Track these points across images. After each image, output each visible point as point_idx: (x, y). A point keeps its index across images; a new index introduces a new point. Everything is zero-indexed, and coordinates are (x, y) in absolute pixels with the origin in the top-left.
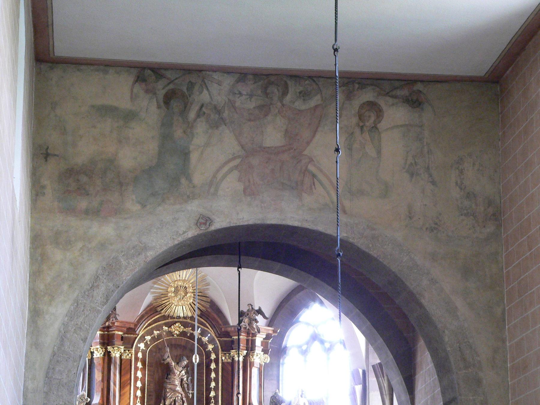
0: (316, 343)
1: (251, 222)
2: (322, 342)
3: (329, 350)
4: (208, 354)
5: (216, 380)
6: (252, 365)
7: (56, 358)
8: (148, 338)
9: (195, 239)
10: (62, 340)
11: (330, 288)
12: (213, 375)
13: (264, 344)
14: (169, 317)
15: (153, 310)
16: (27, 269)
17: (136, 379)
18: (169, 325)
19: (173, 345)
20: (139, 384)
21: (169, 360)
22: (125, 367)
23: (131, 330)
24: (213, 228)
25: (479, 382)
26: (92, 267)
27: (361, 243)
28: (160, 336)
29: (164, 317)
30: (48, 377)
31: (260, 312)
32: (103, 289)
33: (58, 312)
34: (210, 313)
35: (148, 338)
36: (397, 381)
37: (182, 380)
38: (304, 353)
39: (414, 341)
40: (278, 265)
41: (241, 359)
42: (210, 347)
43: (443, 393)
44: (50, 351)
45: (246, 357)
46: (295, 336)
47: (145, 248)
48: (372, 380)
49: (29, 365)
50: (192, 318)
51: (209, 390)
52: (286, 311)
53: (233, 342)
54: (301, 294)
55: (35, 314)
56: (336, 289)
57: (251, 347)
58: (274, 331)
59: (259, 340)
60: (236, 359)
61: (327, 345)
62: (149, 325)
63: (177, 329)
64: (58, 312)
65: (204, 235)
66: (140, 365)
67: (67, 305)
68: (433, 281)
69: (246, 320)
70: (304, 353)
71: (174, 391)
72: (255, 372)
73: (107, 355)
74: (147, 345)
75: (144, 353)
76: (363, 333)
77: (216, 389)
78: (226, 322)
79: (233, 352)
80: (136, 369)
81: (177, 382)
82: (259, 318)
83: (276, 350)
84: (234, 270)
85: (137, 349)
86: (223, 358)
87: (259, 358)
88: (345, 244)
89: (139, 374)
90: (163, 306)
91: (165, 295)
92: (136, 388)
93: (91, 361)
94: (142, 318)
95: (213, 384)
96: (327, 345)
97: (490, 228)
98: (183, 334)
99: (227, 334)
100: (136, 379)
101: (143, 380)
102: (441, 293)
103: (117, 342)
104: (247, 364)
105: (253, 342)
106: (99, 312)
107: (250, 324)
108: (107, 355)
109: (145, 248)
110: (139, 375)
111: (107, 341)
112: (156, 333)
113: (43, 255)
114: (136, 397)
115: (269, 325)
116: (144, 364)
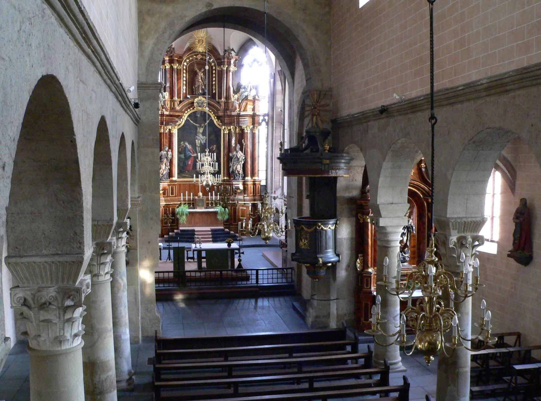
0: (256, 63)
1: (229, 6)
2: (258, 62)
3: (261, 65)
4: (212, 67)
5: (215, 77)
6: (230, 71)
7: (151, 61)
8: (188, 60)
9: (206, 12)
10: (152, 54)
11: (261, 37)
12: (214, 75)
13: (235, 63)
14: (196, 52)
15: (189, 49)
16: (137, 24)
17: (183, 77)
18: (196, 55)
19: (198, 64)
20: (185, 79)
21: (196, 69)
22: (179, 72)
23: (181, 57)
24: (213, 8)
25: (320, 71)
26: (163, 24)
27: (274, 15)
28: (192, 60)
29: (194, 52)
30: (147, 69)
31: (233, 50)
32: (168, 33)
33: (150, 43)
34: (213, 51)
35: (188, 60)
36: (287, 74)
37: (202, 77)
38: (250, 66)
39: (295, 58)
40: (240, 27)
41: (225, 69)
42: (213, 64)
43: (306, 76)
44: (148, 59)
45: (227, 68)
46: (247, 60)
47: (185, 16)
48: (278, 77)
49: (139, 64)
50: (205, 52)
51: (212, 81)
52: (243, 49)
53: (222, 62)
54: (249, 43)
55: (141, 44)
56: (264, 36)
57: (229, 64)
58: (239, 58)
59: (232, 61)
60: (246, 131)
61: (260, 63)
62: (191, 54)
63: (199, 57)
64: (150, 43)
65: (209, 11)
66: (185, 71)
67: (154, 40)
68: (303, 30)
69: (227, 53)
70: (250, 66)
71: (199, 82)
72: (231, 74)
73: (172, 68)
74: (187, 63)
75: (186, 66)
76: (275, 55)
77: (215, 81)
78: (219, 54)
79: (222, 66)
80: (183, 73)
81: (200, 78)
82: (232, 52)
83: (239, 65)
84: (223, 29)
85: (184, 65)
86: (218, 69)
87: (232, 68)
88: (268, 15)
89: (185, 75)
90: (193, 48)
91: (194, 43)
92: (183, 81)
93: (165, 70)
94: (185, 52)
95: (214, 79)
96: (260, 63)
97: (327, 9)
98: (202, 59)
99: (220, 59)
100: (183, 77)
101: (186, 77)
102: (306, 35)
103: (176, 62)
104: (228, 71)
105: (230, 62)
106: (166, 43)
107: (229, 55)
108: (172, 68)
109: (185, 16)
110: (184, 76)
111: (171, 62)
112: (191, 58)
113: (143, 19)
114: (183, 84)
115: (237, 55)
116: (186, 71)
